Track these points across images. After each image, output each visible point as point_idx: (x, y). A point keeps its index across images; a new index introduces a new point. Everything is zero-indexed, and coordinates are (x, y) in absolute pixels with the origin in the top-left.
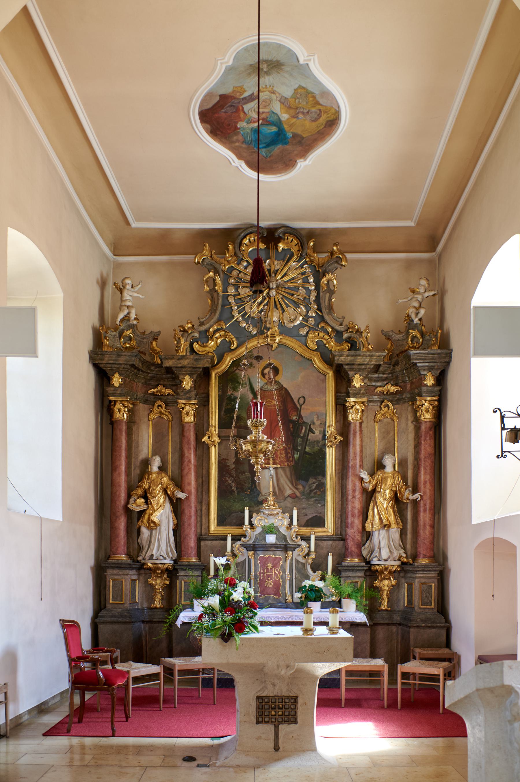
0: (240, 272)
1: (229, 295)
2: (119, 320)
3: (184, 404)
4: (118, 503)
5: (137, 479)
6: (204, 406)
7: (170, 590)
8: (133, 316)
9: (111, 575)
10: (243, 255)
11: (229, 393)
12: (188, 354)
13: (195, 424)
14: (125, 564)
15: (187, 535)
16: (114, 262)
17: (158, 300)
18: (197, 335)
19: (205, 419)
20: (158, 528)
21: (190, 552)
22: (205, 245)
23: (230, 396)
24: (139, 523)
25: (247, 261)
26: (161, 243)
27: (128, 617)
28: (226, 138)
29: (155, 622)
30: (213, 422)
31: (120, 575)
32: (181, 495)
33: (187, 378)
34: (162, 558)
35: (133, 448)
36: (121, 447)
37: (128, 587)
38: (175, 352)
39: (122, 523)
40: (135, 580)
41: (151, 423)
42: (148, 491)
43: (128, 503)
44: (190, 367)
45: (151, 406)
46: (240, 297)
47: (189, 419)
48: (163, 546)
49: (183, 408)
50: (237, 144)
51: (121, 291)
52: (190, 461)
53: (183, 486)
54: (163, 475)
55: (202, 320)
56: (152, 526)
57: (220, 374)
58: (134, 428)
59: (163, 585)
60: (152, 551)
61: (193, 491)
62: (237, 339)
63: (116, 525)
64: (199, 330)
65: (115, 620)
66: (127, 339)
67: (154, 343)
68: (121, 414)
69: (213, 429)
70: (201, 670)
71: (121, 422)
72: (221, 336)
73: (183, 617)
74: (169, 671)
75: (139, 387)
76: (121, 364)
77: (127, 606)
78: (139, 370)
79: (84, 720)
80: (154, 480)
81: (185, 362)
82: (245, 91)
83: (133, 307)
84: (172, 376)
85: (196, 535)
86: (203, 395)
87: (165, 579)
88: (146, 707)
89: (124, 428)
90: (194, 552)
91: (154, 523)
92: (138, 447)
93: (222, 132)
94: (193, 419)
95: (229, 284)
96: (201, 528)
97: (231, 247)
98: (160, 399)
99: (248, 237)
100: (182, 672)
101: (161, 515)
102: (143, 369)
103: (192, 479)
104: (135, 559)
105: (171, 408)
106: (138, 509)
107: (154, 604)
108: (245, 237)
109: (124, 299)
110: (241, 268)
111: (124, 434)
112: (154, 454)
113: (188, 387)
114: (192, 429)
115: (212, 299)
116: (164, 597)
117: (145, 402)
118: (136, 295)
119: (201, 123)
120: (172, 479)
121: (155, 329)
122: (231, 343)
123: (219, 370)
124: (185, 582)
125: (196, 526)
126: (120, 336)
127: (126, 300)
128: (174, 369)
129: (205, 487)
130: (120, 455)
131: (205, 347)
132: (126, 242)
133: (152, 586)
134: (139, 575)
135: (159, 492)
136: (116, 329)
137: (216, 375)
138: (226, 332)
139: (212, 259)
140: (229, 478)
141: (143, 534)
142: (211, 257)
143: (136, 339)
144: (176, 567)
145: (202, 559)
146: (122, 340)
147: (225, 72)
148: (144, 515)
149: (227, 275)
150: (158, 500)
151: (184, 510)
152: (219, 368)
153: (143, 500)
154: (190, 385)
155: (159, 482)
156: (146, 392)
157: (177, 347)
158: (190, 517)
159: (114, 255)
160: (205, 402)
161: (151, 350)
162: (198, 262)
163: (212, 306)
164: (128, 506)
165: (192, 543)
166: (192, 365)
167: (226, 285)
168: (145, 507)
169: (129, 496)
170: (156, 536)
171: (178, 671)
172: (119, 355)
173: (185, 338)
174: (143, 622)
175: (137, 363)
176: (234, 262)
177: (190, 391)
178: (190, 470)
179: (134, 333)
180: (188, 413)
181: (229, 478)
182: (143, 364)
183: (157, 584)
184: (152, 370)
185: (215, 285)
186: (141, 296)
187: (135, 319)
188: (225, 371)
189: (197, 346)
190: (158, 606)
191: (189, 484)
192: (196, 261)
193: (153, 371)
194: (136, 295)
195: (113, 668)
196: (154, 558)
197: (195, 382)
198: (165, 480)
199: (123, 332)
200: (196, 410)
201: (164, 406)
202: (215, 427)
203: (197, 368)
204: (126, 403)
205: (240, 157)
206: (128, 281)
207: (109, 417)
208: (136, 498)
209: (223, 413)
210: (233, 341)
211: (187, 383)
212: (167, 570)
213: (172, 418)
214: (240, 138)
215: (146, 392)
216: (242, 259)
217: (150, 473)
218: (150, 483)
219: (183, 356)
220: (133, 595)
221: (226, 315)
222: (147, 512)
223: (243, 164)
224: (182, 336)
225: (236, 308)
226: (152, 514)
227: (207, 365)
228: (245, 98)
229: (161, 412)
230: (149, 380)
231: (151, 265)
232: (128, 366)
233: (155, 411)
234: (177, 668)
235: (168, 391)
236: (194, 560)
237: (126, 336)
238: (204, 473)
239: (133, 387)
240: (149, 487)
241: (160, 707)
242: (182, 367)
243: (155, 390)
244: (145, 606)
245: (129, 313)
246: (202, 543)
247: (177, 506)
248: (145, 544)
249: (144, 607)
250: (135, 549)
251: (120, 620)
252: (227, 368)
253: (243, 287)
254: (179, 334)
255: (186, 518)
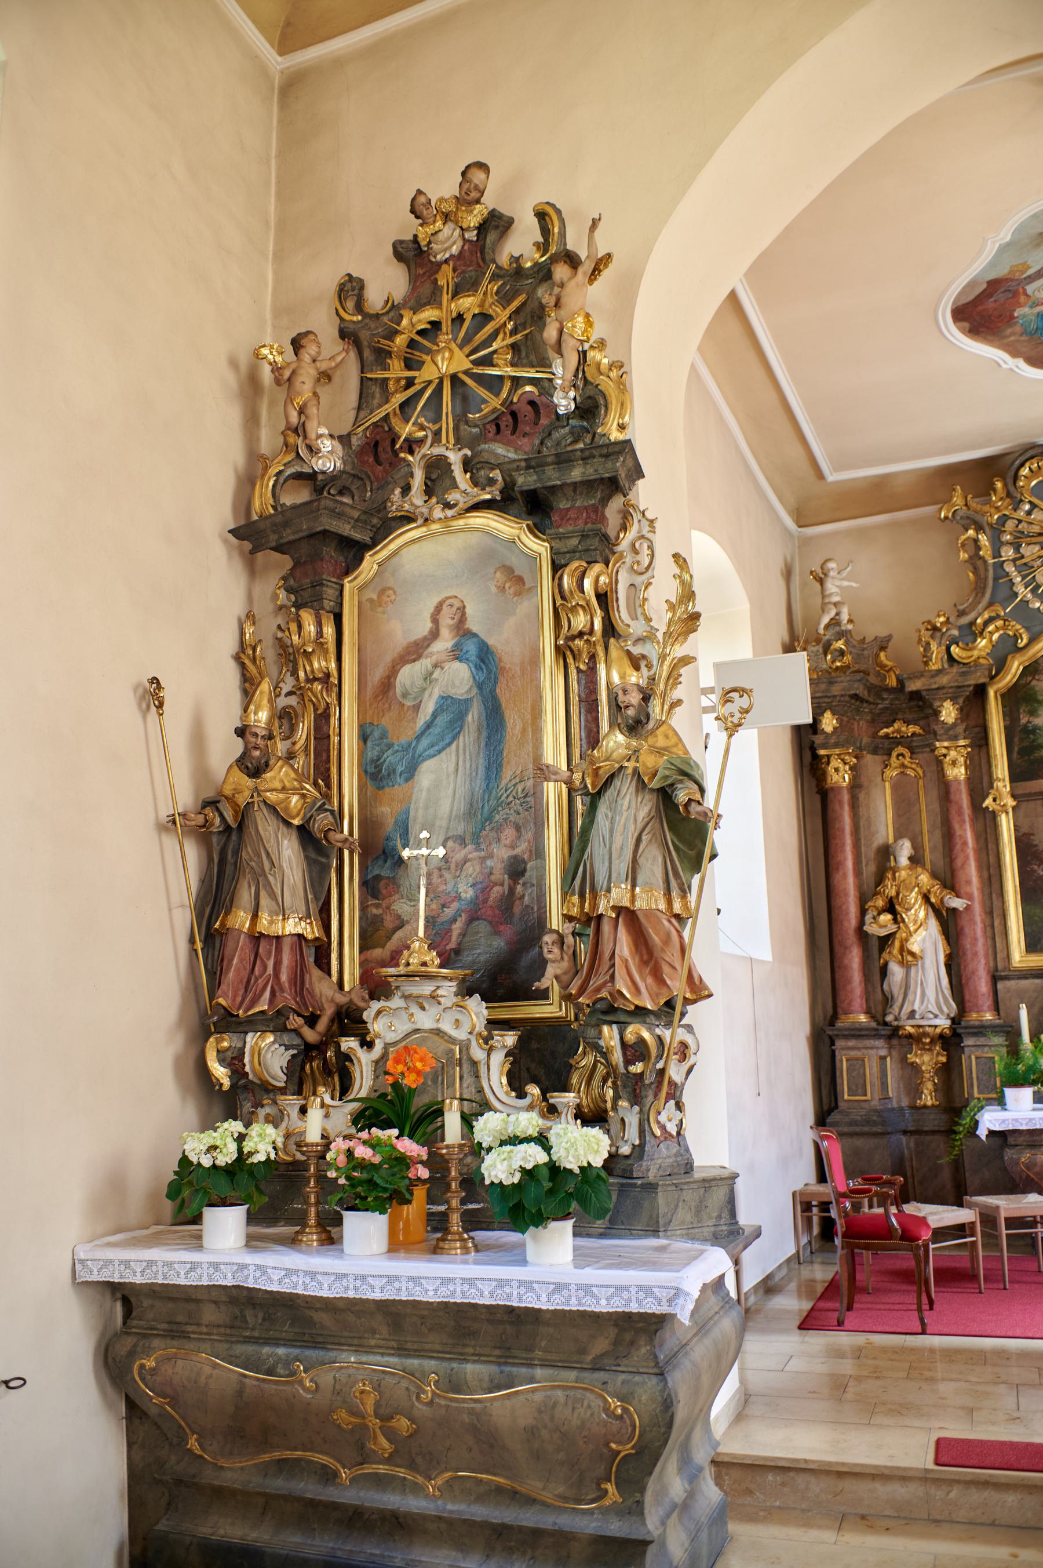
0: (1020, 521)
1: (1004, 561)
2: (822, 626)
3: (946, 748)
4: (846, 924)
5: (873, 879)
6: (980, 746)
7: (949, 1073)
8: (845, 617)
9: (843, 1049)
10: (1022, 494)
11: (1023, 721)
12: (946, 666)
13: (969, 780)
14: (867, 1029)
15: (973, 973)
16: (799, 538)
17: (885, 586)
18: (955, 632)
19: (984, 770)
20: (920, 963)
21: (980, 1002)
22: (954, 490)
23: (1026, 726)
24: (885, 955)
25: (1030, 502)
26: (876, 496)
27: (877, 1125)
28: (994, 334)
29: (927, 1133)
30: (999, 772)
31: (859, 1049)
32: (957, 903)
33: (948, 704)
34: (931, 1016)
35: (862, 830)
36: (843, 831)
37: (875, 1070)
38: (922, 665)
39: (854, 959)
40: (883, 1058)
41: (887, 784)
42: (895, 901)
43: (862, 922)
44: (951, 687)
45: (885, 757)
46: (1023, 561)
47: (958, 772)
48: (931, 993)
49: (945, 756)
50: (1012, 338)
51: (821, 581)
52: (965, 843)
53: (957, 886)
54: (920, 870)
55: (961, 608)
56: (910, 959)
57: (1004, 690)
58: (862, 796)
59: (936, 1064)
60: (913, 1004)
61: (976, 893)
62: (1027, 629)
63: (846, 962)
64: (958, 624)
65: (857, 1129)
66: (837, 654)
67: (882, 655)
68: (839, 775)
69: (1000, 784)
70: (1039, 1219)
71: (840, 788)
72: (997, 629)
73: (990, 1121)
74: (989, 1219)
75: (861, 726)
76: (835, 696)
77: (875, 1103)
78: (862, 700)
79: (855, 1306)
80: (904, 881)
81: (944, 680)
82: (1029, 267)
83: (843, 603)
84: (921, 706)
85: (989, 971)
86: (976, 730)
87: (938, 1054)
88: (944, 1287)
89: (846, 797)
90: (987, 1002)
91: (912, 954)
92: (869, 827)
93: (987, 328)
94: (963, 771)
95: (1002, 543)
96: (995, 958)
97: (999, 485)
98: (899, 744)
99: (1027, 465)
100: (1011, 1222)
101: (924, 940)
102: (871, 700)
103: (971, 873)
104: (880, 1019)
105: (920, 756)
106: (883, 933)
107: (921, 1099)
108: (1022, 465)
109: (827, 593)
110: (1021, 514)
111: (846, 808)
112: (899, 836)
113: (950, 720)
114: (963, 788)
115: (975, 571)
116: (939, 1086)
117: (875, 751)
118: (846, 583)
119: (955, 322)
120: (934, 875)
121: (880, 631)
122: (1016, 637)
123: (1001, 685)
124: (977, 1058)
125: (986, 956)
126: (826, 649)
127: (831, 595)
128: (924, 693)
129: (995, 886)
130: (843, 844)
131: (970, 650)
132: (816, 503)
133: (915, 1068)
134: (890, 1048)
135: (916, 900)
136: (818, 641)
137: (996, 693)
138: (1005, 621)
139: (969, 509)
140: (1039, 866)
141: (893, 975)
142: (966, 505)
143: (851, 653)
144: (959, 1031)
145: (1002, 1013)
146: (829, 657)
147: (998, 250)
148: (893, 942)
149: (996, 531)
150: (916, 915)
151: (962, 929)
152: (1000, 680)
153: (889, 917)
154: (953, 715)
155: (913, 884)
156: (875, 735)
157: (924, 656)
158: (976, 939)
159: (800, 527)
160: (981, 741)
161: (878, 665)
162: (946, 518)
163: (976, 582)
164: (865, 928)
165: (983, 986)
166: (956, 684)
167: (997, 546)
168: (893, 928)
169: (863, 912)
170: (917, 976)
171: (1006, 1219)
172: (831, 683)
173: (938, 640)
174: (905, 1132)
175: (861, 690)
176: (1007, 508)
177: (954, 725)
178: (967, 858)
179: (846, 644)
180: (954, 763)
181: (1039, 866)
182: (869, 692)
183: (923, 1063)
184: (883, 699)
185: (978, 548)
186: (854, 585)
187: (850, 621)
188: (1011, 684)
189: (957, 650)
190: (929, 1103)
191: (969, 882)
192: (942, 515)
193: (886, 699)
194: (846, 583)
195: (899, 1211)
196: (917, 1016)
197: (961, 710)
198: (924, 878)
199: (831, 645)
200: (969, 756)
201: (907, 753)
202: (1004, 780)
203: (963, 686)
204: (847, 757)
205: (1014, 354)
206: (831, 565)
207: (814, 783)
208: (875, 913)
209: (1015, 756)
210: (1021, 635)
211: (949, 713)
212: (941, 1036)
213: (924, 772)
214: (1018, 329)
215: (875, 735)
216: (1021, 501)
217: (894, 870)
218: (898, 886)
219: (939, 672)
220: (884, 1085)
221: (1003, 593)
222: (898, 935)
223: (1021, 363)
224: (932, 637)
225: (1019, 579)
226: (907, 940)
227: (982, 680)
228: (1029, 277)
229: (903, 766)
230: (879, 714)
231: (861, 532)
232: (847, 699)
233: (894, 765)
234: (1003, 1214)
235: (912, 729)
236: (989, 1016)
237: (836, 650)
238: (992, 860)
239: (852, 730)
240: (898, 894)
241: (980, 1288)
242: (938, 689)
243: (890, 730)
244: (905, 1102)
245: (837, 614)
246: (1000, 985)
247: (950, 924)
248: (897, 992)
249: (903, 1105)
250: (881, 1003)
251: (866, 1129)
252: (1015, 680)
253: (1028, 544)
254: (926, 635)
255: (967, 943)
